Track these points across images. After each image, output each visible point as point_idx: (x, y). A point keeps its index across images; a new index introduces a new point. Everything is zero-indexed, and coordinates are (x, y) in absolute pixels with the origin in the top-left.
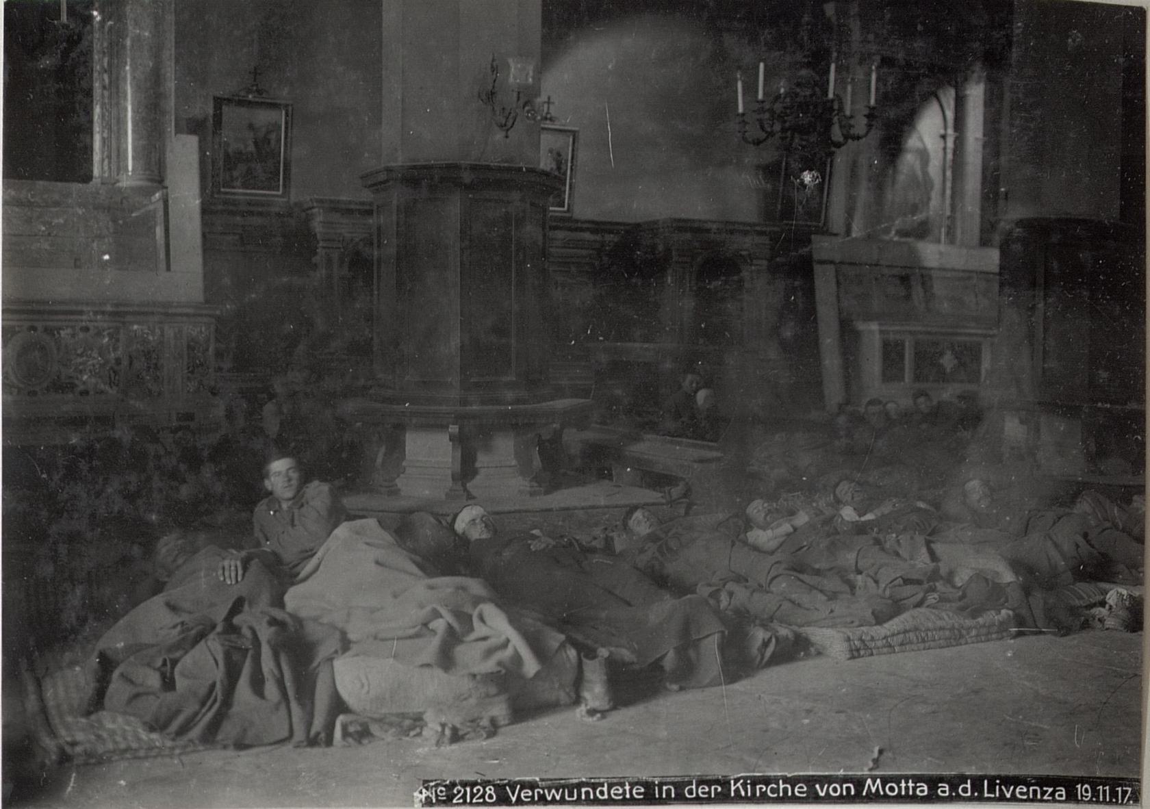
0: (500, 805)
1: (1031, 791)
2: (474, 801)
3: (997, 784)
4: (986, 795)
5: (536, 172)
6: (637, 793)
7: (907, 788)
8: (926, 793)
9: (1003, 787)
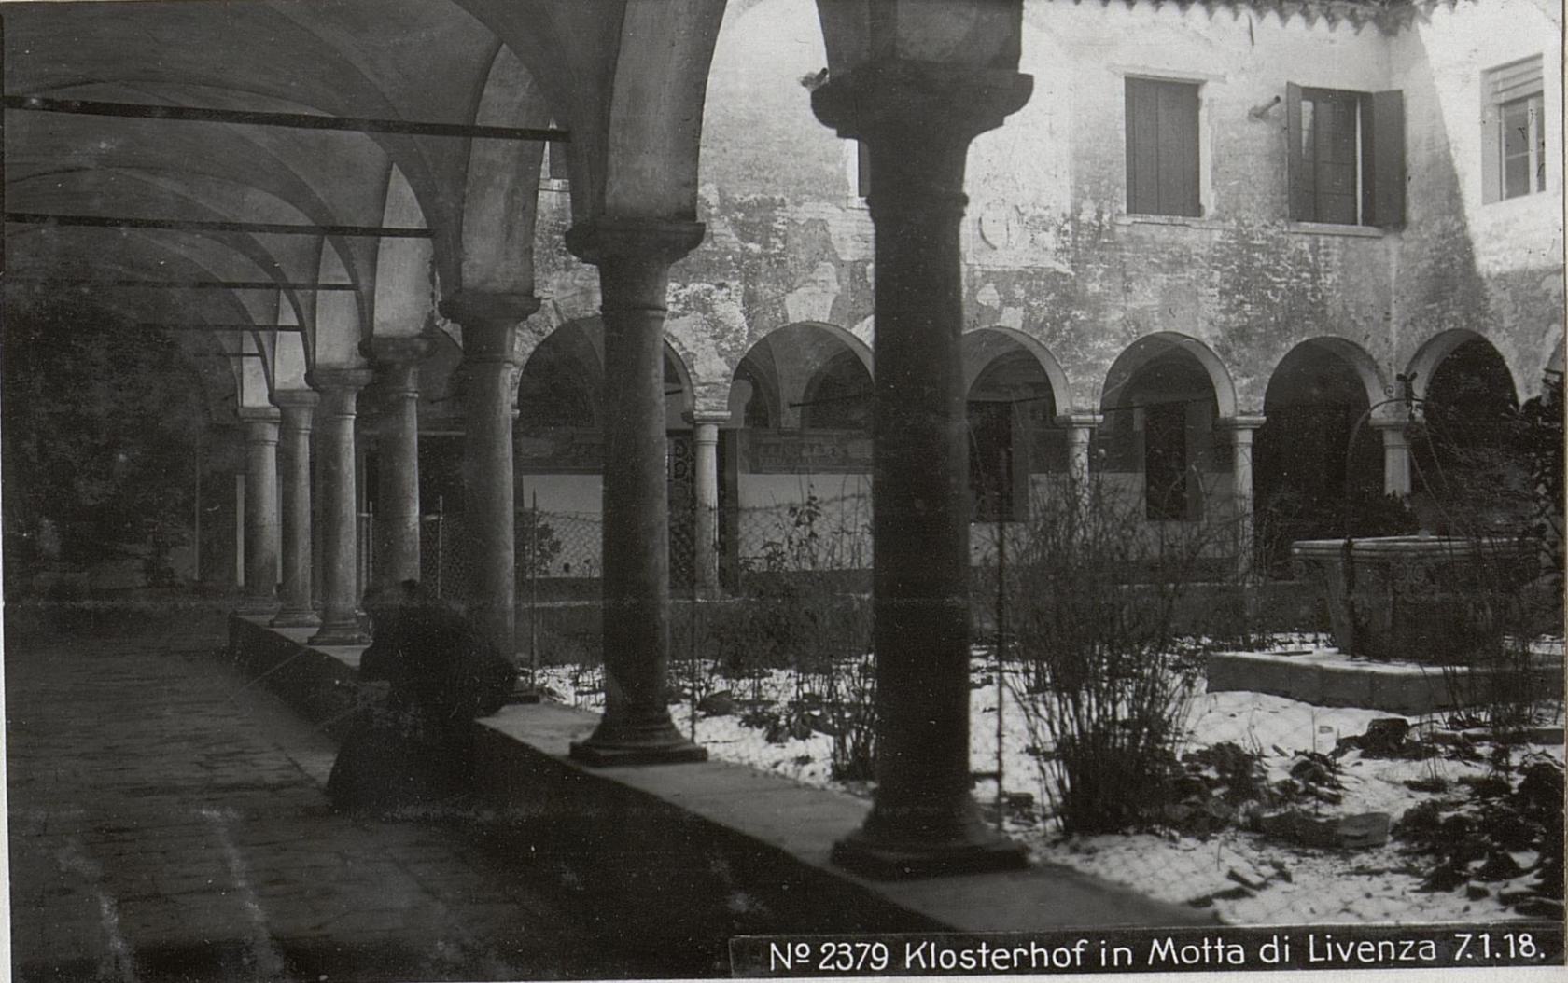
0: (891, 975)
2: (1402, 957)
3: (1102, 946)
4: (1313, 959)
6: (1363, 954)
7: (1213, 953)
9: (1339, 945)
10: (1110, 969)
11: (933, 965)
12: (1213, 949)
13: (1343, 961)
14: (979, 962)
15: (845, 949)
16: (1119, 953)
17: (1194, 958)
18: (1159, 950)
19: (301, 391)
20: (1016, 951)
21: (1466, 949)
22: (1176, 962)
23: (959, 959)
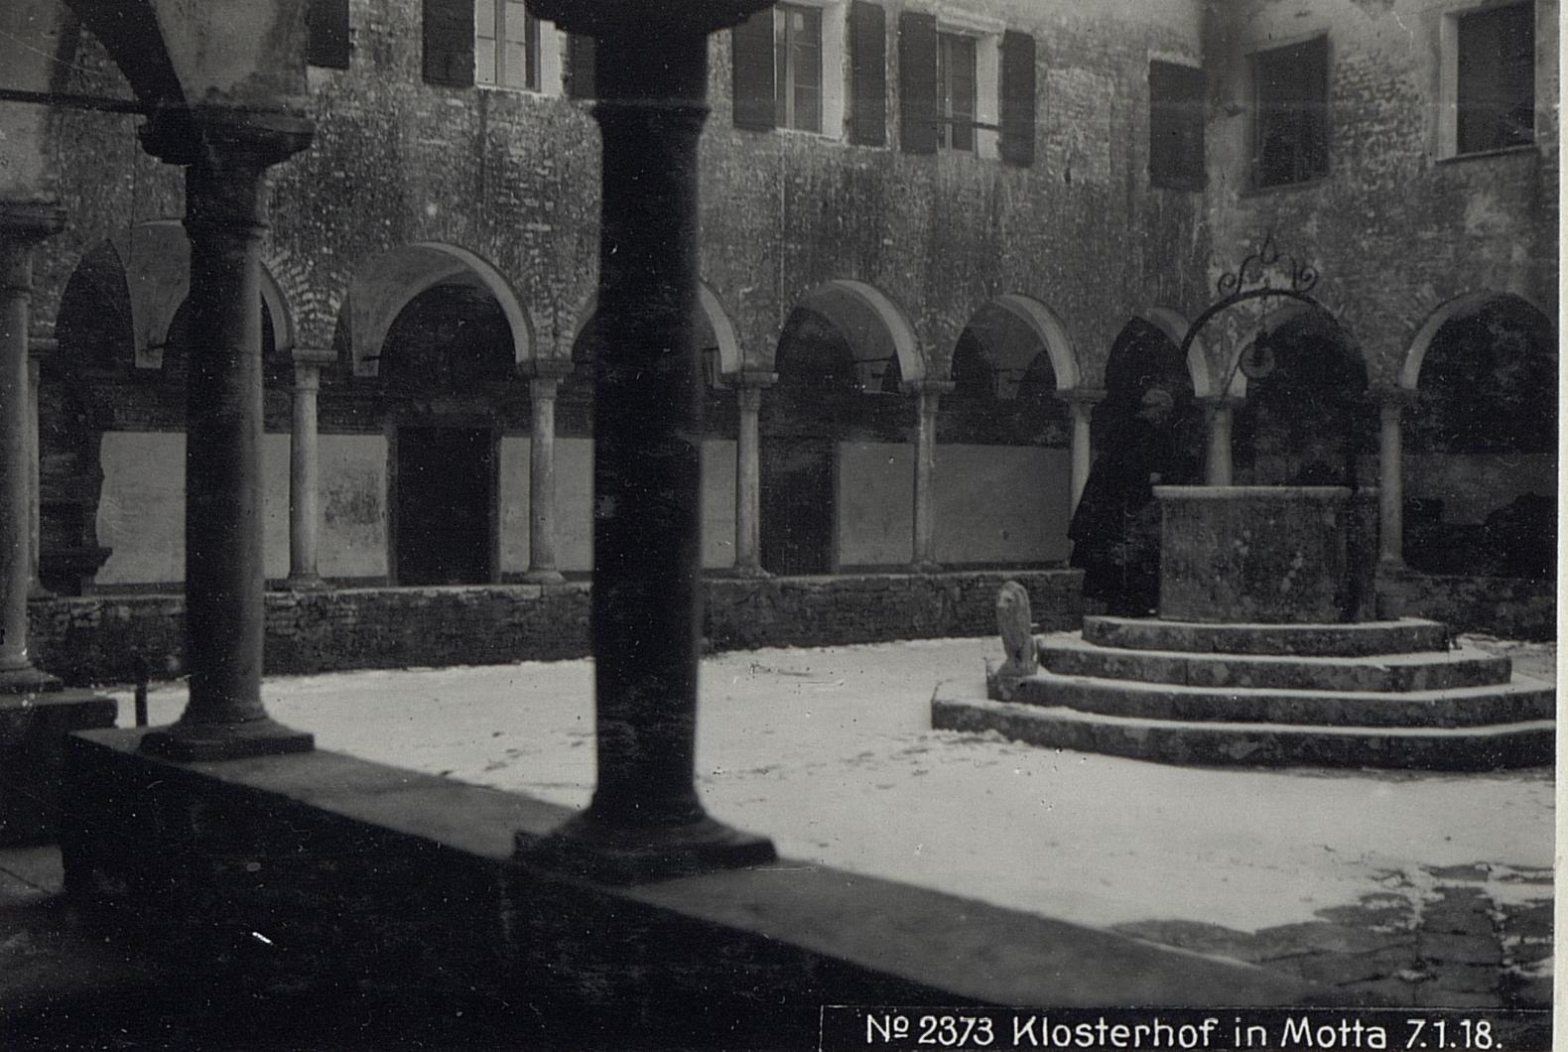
5: (504, 598)
7: (1351, 1036)
8: (1383, 1046)
11: (1045, 1043)
14: (1097, 1039)
15: (985, 1024)
20: (1137, 1029)
21: (1418, 1037)
22: (1310, 1044)
23: (1074, 1036)
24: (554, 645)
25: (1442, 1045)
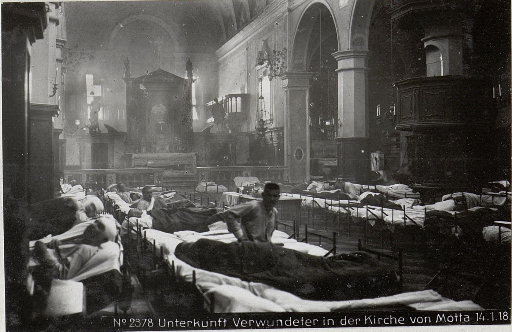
1: (356, 321)
7: (458, 318)
10: (326, 326)
12: (222, 322)
13: (235, 326)
16: (329, 321)
17: (451, 321)
18: (440, 317)
19: (158, 249)
24: (211, 222)
25: (493, 320)
